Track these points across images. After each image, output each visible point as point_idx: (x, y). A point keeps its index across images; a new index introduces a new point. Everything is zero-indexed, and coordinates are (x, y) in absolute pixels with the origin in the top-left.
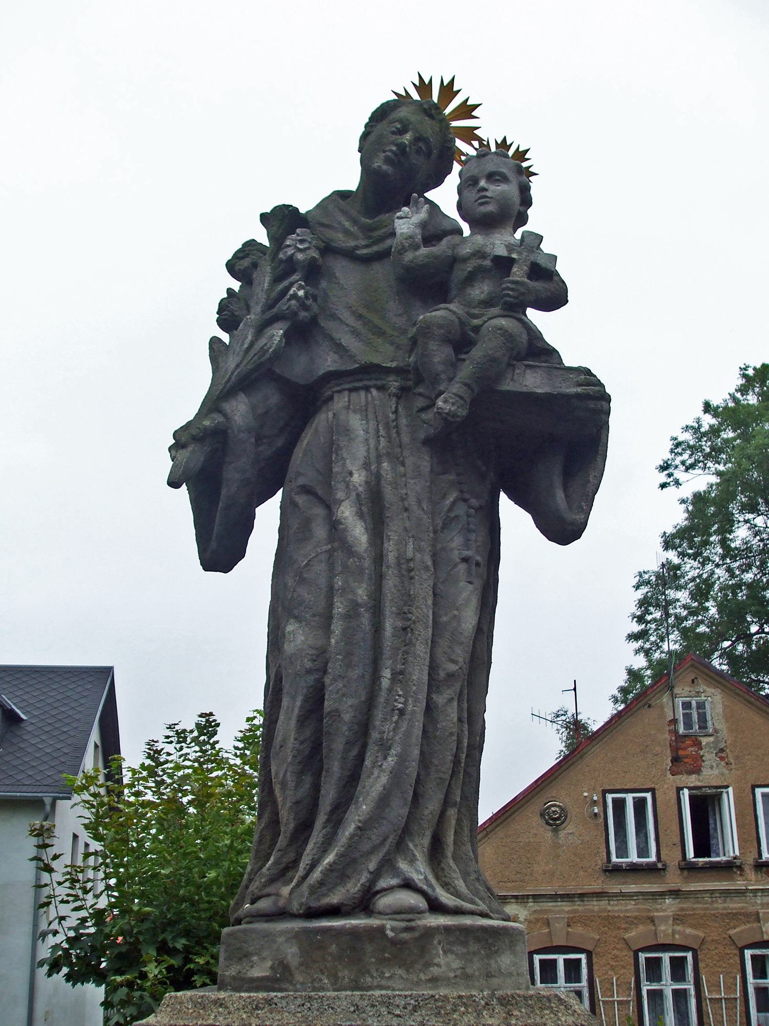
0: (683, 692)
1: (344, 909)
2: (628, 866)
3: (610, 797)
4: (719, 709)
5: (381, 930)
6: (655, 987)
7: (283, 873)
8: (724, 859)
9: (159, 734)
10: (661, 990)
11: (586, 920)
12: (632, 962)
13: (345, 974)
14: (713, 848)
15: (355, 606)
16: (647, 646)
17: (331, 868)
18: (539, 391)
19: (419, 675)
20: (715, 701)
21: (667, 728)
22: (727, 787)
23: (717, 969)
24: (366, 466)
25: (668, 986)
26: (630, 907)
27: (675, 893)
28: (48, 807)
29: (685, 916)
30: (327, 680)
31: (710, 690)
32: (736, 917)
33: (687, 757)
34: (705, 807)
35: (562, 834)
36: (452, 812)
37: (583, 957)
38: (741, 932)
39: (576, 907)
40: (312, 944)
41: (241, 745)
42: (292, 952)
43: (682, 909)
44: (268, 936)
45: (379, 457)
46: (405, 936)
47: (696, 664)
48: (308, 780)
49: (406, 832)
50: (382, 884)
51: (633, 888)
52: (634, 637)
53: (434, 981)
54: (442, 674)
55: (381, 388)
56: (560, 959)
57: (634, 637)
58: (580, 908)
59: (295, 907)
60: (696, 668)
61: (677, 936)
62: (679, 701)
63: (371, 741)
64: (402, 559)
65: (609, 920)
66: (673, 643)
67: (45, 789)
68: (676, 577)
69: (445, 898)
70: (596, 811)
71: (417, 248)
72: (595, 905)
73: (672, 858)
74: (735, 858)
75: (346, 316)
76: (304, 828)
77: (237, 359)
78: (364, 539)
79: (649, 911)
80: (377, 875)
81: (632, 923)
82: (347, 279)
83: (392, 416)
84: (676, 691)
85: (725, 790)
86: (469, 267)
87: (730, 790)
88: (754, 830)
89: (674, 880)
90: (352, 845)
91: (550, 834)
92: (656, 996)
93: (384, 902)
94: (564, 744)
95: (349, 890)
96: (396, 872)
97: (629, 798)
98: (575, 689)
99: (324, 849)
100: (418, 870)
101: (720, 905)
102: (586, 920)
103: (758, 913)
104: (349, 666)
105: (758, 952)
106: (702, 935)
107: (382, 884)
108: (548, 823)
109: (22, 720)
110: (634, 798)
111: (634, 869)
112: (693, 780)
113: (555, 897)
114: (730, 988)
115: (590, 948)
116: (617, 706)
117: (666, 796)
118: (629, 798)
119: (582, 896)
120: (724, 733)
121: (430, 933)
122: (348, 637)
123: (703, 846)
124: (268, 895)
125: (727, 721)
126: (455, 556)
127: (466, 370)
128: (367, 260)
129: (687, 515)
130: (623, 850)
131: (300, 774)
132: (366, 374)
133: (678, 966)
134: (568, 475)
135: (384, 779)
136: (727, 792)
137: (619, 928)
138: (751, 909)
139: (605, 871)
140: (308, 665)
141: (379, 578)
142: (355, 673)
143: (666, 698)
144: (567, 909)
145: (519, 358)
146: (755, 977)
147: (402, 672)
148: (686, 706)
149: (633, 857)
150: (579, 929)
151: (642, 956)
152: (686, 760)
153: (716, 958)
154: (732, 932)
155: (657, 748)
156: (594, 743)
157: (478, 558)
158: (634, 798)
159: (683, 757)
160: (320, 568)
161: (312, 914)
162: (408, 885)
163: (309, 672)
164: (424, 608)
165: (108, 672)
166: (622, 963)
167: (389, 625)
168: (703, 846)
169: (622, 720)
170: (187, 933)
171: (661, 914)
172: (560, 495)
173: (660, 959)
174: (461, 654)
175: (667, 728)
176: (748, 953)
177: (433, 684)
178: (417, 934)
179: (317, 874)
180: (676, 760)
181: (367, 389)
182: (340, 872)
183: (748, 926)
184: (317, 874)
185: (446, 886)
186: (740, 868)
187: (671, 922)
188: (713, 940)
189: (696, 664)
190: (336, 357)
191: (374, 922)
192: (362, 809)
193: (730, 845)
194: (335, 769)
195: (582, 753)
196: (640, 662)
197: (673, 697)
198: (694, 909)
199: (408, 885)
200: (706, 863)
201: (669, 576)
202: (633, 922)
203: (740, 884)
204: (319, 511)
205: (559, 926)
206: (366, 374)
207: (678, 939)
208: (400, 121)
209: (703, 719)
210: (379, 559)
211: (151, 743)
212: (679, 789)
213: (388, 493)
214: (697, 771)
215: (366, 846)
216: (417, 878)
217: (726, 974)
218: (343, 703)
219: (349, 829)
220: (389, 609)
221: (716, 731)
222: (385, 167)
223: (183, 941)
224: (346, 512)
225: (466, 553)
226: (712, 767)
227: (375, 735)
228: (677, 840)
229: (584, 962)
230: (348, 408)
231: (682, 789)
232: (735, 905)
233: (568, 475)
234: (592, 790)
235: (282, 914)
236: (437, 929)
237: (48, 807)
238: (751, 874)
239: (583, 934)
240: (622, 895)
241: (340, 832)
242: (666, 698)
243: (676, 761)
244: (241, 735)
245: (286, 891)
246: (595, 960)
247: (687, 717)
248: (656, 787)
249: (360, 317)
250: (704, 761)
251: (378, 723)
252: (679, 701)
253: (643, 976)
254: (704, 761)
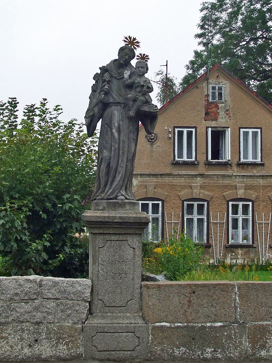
1: (113, 199)
2: (182, 162)
3: (176, 130)
4: (228, 90)
5: (119, 202)
6: (190, 217)
7: (103, 192)
8: (224, 160)
10: (193, 219)
11: (162, 186)
12: (181, 205)
13: (113, 209)
14: (220, 155)
15: (116, 148)
16: (205, 41)
17: (111, 192)
18: (147, 111)
19: (125, 160)
20: (226, 86)
21: (204, 99)
22: (228, 128)
23: (217, 210)
24: (117, 122)
26: (182, 181)
27: (202, 175)
29: (205, 186)
30: (111, 161)
31: (225, 82)
32: (227, 187)
34: (218, 136)
35: (155, 146)
36: (129, 182)
37: (160, 202)
38: (229, 194)
39: (159, 180)
40: (109, 204)
41: (26, 111)
42: (105, 205)
43: (204, 183)
44: (102, 203)
45: (120, 120)
46: (122, 203)
47: (219, 69)
48: (107, 177)
49: (122, 186)
50: (118, 195)
51: (184, 172)
52: (199, 36)
53: (126, 210)
54: (128, 160)
55: (120, 106)
56: (150, 203)
57: (199, 36)
58: (160, 181)
59: (105, 198)
60: (219, 70)
61: (201, 195)
62: (210, 86)
63: (117, 172)
64: (123, 141)
65: (173, 187)
70: (170, 136)
71: (128, 80)
72: (167, 180)
74: (229, 160)
75: (115, 91)
77: (96, 100)
78: (117, 136)
79: (190, 183)
80: (118, 193)
82: (115, 84)
83: (122, 112)
84: (210, 81)
85: (227, 129)
86: (137, 85)
87: (229, 129)
88: (238, 148)
89: (202, 169)
90: (114, 189)
91: (149, 146)
92: (190, 221)
93: (119, 198)
94: (160, 90)
95: (114, 195)
96: (121, 193)
97: (185, 131)
98: (167, 65)
99: (110, 188)
100: (124, 193)
101: (221, 182)
102: (162, 186)
103: (236, 186)
104: (114, 159)
105: (235, 203)
106: (212, 195)
107: (118, 195)
108: (148, 141)
110: (187, 131)
111: (185, 164)
112: (214, 124)
113: (149, 175)
115: (163, 199)
116: (188, 71)
117: (201, 130)
118: (185, 131)
119: (161, 175)
120: (229, 102)
121: (126, 203)
122: (114, 154)
123: (216, 153)
124: (100, 196)
126: (131, 138)
127: (135, 107)
128: (119, 79)
131: (105, 176)
134: (151, 123)
135: (119, 178)
136: (228, 130)
137: (176, 190)
138: (234, 184)
140: (108, 158)
141: (119, 143)
142: (115, 160)
143: (205, 84)
145: (145, 103)
146: (233, 214)
147: (122, 160)
148: (214, 88)
149: (185, 158)
150: (159, 190)
151: (186, 203)
152: (211, 114)
154: (224, 194)
155: (199, 108)
156: (172, 103)
157: (135, 138)
158: (187, 131)
159: (210, 112)
160: (110, 141)
162: (122, 195)
163: (108, 160)
164: (126, 149)
166: (177, 206)
167: (121, 152)
168: (216, 153)
169: (184, 93)
171: (195, 184)
173: (193, 205)
174: (132, 155)
175: (204, 99)
176: (231, 203)
177: (127, 162)
178: (124, 203)
180: (207, 114)
181: (118, 106)
182: (112, 193)
183: (232, 191)
185: (127, 194)
186: (231, 165)
187: (199, 188)
188: (216, 197)
189: (219, 69)
190: (113, 99)
191: (118, 201)
193: (227, 155)
194: (111, 176)
195: (165, 109)
197: (208, 84)
198: (209, 183)
199: (122, 195)
200: (216, 162)
202: (183, 187)
203: (230, 172)
204: (109, 129)
205: (151, 188)
207: (201, 196)
208: (126, 53)
209: (220, 94)
210: (119, 140)
212: (207, 128)
213: (121, 128)
214: (216, 119)
215: (116, 189)
216: (123, 194)
217: (220, 212)
218: (113, 165)
219: (114, 186)
221: (226, 101)
222: (123, 62)
225: (133, 137)
226: (222, 118)
227: (118, 171)
228: (205, 151)
229: (160, 205)
230: (114, 109)
231: (209, 127)
232: (227, 182)
233: (151, 123)
234: (169, 126)
235: (103, 199)
236: (127, 202)
238: (235, 168)
239: (161, 193)
240: (261, 104)
241: (112, 186)
242: (205, 84)
243: (207, 114)
244: (26, 107)
245: (103, 195)
247: (213, 93)
248: (197, 126)
249: (117, 92)
250: (219, 115)
251: (118, 169)
252: (210, 86)
253: (185, 212)
254: (219, 115)
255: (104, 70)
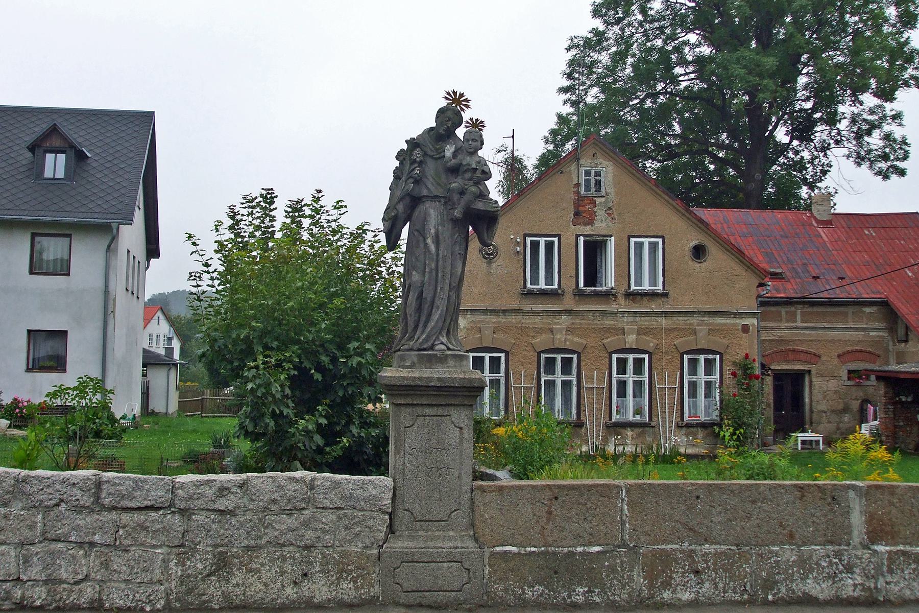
0: (586, 163)
3: (529, 239)
4: (610, 177)
6: (550, 378)
7: (411, 338)
8: (605, 288)
9: (237, 201)
10: (554, 381)
14: (598, 280)
19: (447, 288)
22: (611, 236)
25: (559, 378)
27: (569, 312)
28: (115, 231)
31: (605, 163)
32: (608, 330)
33: (585, 212)
34: (595, 249)
35: (494, 266)
37: (502, 355)
40: (421, 357)
42: (415, 359)
43: (573, 324)
44: (410, 355)
51: (540, 307)
52: (565, 90)
56: (487, 356)
57: (565, 90)
58: (503, 320)
62: (583, 170)
64: (444, 257)
65: (523, 330)
66: (593, 96)
67: (112, 216)
68: (599, 42)
69: (451, 346)
72: (513, 319)
73: (569, 286)
76: (416, 327)
79: (550, 324)
81: (538, 332)
84: (582, 162)
87: (613, 238)
89: (569, 302)
92: (551, 385)
93: (437, 348)
95: (430, 344)
98: (513, 137)
99: (422, 333)
100: (444, 340)
101: (599, 322)
103: (624, 329)
105: (621, 356)
106: (585, 343)
108: (484, 257)
109: (88, 157)
111: (543, 293)
112: (587, 230)
113: (485, 312)
114: (600, 380)
115: (507, 349)
117: (568, 239)
118: (542, 241)
120: (612, 196)
122: (429, 279)
123: (592, 277)
125: (615, 187)
127: (463, 203)
128: (436, 159)
129: (564, 115)
130: (535, 280)
132: (435, 198)
133: (567, 363)
134: (488, 229)
138: (620, 325)
139: (522, 294)
141: (437, 261)
144: (494, 320)
148: (588, 173)
149: (542, 285)
150: (500, 336)
151: (543, 356)
153: (593, 359)
154: (605, 341)
159: (582, 212)
161: (419, 350)
162: (442, 343)
164: (448, 270)
165: (149, 117)
167: (440, 275)
168: (592, 277)
170: (277, 339)
172: (486, 234)
173: (555, 359)
174: (457, 280)
176: (615, 356)
177: (450, 290)
179: (421, 340)
180: (577, 214)
182: (426, 340)
183: (616, 337)
184: (421, 340)
186: (615, 296)
192: (431, 324)
193: (610, 279)
194: (425, 313)
196: (568, 109)
198: (581, 324)
199: (442, 343)
200: (592, 291)
201: (596, 41)
202: (539, 331)
203: (613, 307)
204: (421, 238)
205: (488, 333)
206: (435, 198)
207: (568, 345)
209: (598, 183)
210: (438, 255)
211: (232, 208)
212: (577, 236)
213: (441, 237)
214: (591, 223)
217: (599, 370)
220: (440, 271)
221: (607, 194)
223: (276, 343)
224: (429, 241)
228: (573, 273)
229: (503, 359)
231: (580, 235)
232: (609, 322)
233: (488, 229)
235: (411, 350)
237: (115, 231)
238: (622, 300)
239: (502, 339)
240: (533, 312)
242: (573, 167)
245: (411, 343)
246: (510, 358)
247: (588, 182)
252: (583, 170)
253: (542, 370)
255: (413, 144)
